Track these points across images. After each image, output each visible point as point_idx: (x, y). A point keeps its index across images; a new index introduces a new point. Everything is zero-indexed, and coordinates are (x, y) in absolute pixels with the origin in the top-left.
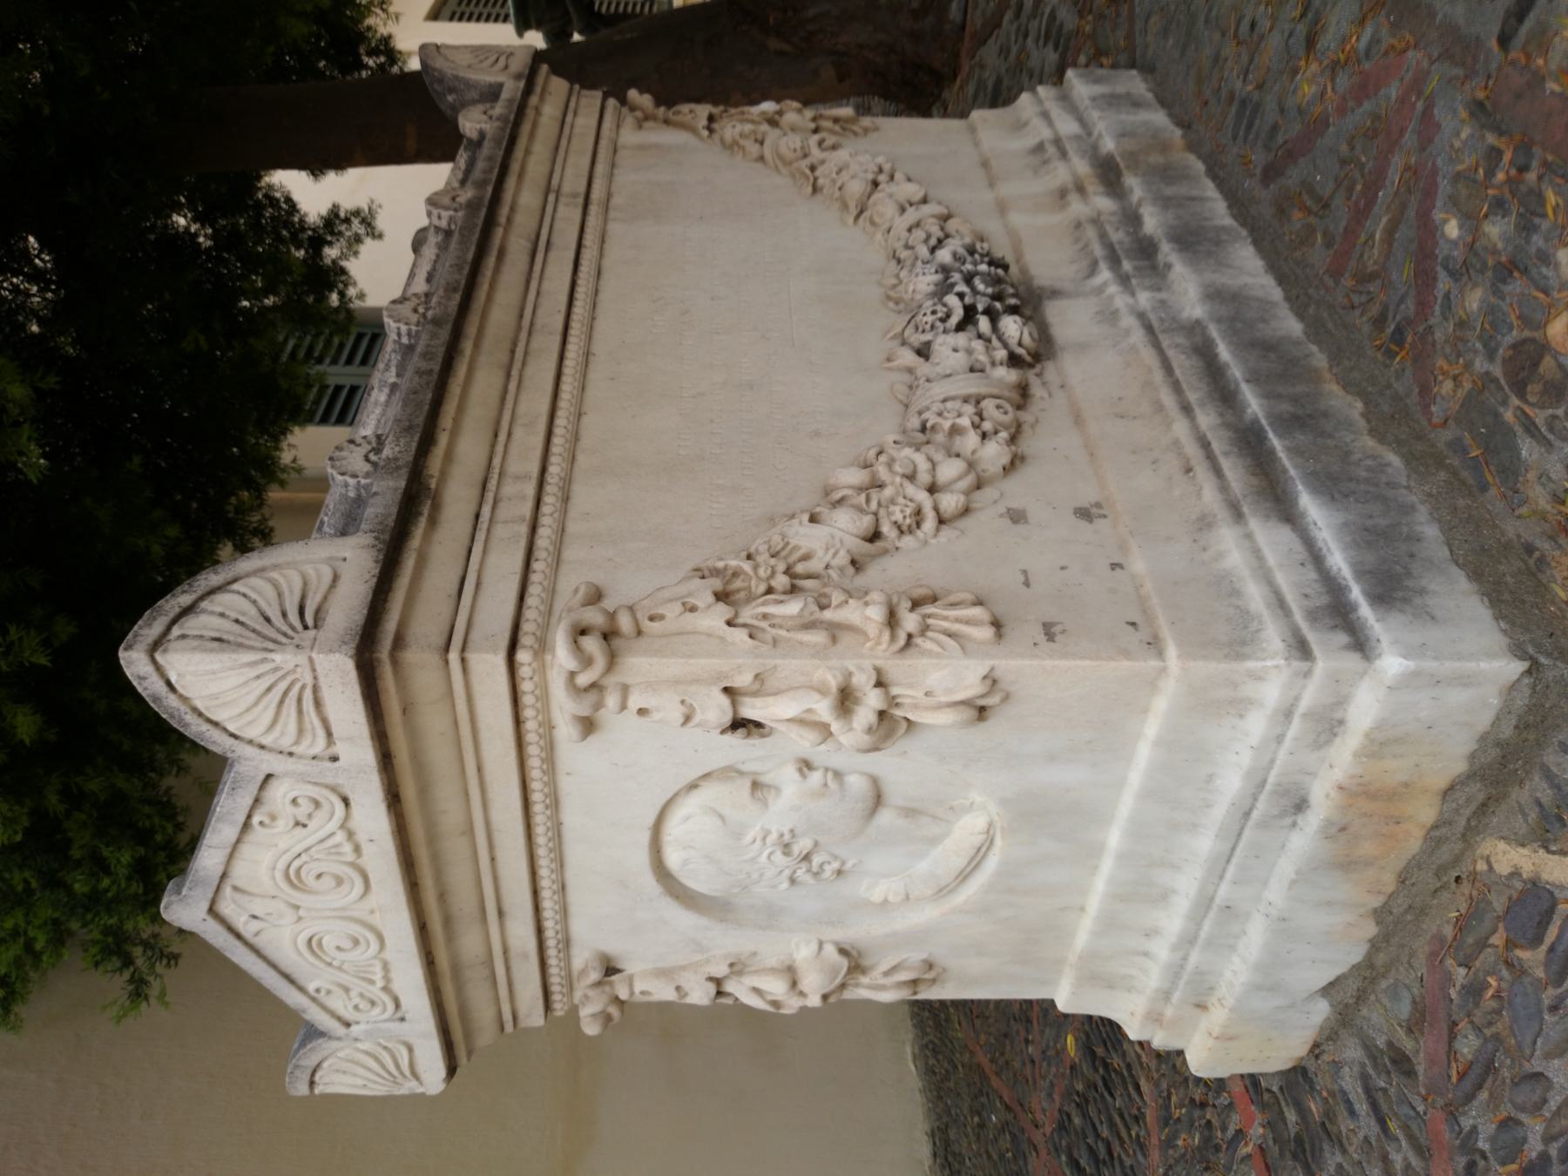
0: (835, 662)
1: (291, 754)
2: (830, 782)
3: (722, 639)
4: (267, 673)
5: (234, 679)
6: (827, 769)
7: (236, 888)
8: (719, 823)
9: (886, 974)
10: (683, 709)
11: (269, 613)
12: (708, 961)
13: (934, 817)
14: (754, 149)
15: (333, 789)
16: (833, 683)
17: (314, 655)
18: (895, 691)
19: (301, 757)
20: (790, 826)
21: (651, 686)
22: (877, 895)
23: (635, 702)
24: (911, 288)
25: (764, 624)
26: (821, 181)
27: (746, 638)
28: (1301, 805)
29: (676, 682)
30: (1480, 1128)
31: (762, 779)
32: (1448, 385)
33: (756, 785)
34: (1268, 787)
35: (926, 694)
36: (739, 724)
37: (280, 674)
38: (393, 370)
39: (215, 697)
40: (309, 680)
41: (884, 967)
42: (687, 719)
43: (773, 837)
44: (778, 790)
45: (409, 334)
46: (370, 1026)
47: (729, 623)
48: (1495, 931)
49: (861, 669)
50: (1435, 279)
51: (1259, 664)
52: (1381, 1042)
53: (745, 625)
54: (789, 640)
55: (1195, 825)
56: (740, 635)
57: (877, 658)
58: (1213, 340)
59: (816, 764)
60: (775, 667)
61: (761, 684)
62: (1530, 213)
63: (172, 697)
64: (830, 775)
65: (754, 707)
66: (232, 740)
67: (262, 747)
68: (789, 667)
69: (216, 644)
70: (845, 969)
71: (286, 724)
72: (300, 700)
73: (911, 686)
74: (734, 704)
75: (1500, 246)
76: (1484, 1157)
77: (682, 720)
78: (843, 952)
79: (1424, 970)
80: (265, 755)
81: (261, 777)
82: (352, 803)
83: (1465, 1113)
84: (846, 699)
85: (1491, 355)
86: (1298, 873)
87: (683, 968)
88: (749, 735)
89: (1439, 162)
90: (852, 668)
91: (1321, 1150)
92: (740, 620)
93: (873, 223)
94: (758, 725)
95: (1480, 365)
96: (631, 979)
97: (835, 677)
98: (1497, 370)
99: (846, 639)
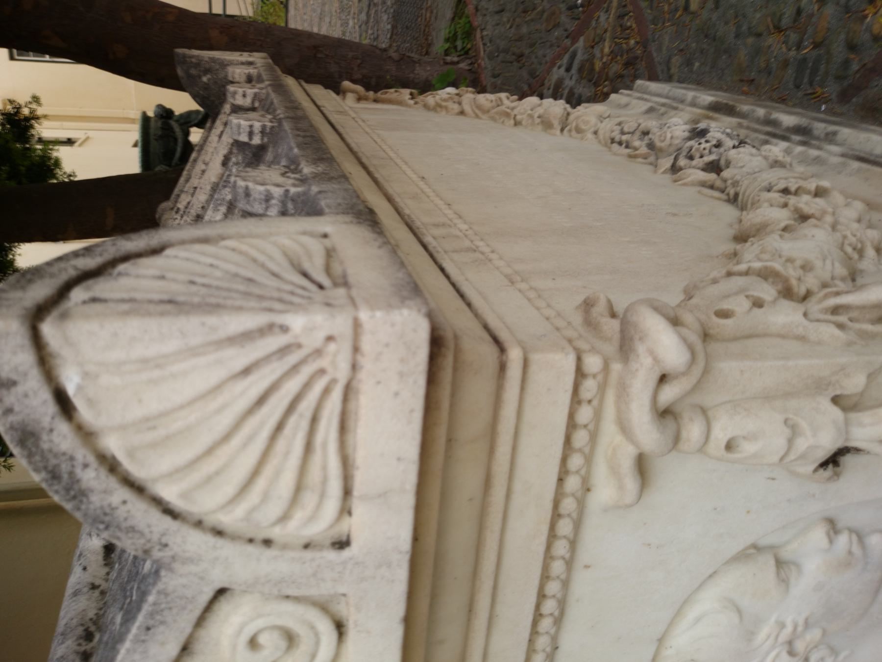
1: (267, 543)
4: (266, 359)
5: (204, 374)
11: (249, 274)
14: (456, 107)
15: (323, 607)
17: (364, 315)
19: (285, 547)
23: (720, 434)
24: (669, 135)
26: (519, 117)
33: (780, 563)
37: (292, 359)
39: (149, 422)
40: (342, 373)
44: (798, 566)
45: (263, 132)
63: (63, 427)
66: (167, 520)
67: (219, 533)
69: (168, 307)
71: (278, 473)
72: (314, 420)
80: (226, 549)
81: (208, 593)
93: (579, 130)
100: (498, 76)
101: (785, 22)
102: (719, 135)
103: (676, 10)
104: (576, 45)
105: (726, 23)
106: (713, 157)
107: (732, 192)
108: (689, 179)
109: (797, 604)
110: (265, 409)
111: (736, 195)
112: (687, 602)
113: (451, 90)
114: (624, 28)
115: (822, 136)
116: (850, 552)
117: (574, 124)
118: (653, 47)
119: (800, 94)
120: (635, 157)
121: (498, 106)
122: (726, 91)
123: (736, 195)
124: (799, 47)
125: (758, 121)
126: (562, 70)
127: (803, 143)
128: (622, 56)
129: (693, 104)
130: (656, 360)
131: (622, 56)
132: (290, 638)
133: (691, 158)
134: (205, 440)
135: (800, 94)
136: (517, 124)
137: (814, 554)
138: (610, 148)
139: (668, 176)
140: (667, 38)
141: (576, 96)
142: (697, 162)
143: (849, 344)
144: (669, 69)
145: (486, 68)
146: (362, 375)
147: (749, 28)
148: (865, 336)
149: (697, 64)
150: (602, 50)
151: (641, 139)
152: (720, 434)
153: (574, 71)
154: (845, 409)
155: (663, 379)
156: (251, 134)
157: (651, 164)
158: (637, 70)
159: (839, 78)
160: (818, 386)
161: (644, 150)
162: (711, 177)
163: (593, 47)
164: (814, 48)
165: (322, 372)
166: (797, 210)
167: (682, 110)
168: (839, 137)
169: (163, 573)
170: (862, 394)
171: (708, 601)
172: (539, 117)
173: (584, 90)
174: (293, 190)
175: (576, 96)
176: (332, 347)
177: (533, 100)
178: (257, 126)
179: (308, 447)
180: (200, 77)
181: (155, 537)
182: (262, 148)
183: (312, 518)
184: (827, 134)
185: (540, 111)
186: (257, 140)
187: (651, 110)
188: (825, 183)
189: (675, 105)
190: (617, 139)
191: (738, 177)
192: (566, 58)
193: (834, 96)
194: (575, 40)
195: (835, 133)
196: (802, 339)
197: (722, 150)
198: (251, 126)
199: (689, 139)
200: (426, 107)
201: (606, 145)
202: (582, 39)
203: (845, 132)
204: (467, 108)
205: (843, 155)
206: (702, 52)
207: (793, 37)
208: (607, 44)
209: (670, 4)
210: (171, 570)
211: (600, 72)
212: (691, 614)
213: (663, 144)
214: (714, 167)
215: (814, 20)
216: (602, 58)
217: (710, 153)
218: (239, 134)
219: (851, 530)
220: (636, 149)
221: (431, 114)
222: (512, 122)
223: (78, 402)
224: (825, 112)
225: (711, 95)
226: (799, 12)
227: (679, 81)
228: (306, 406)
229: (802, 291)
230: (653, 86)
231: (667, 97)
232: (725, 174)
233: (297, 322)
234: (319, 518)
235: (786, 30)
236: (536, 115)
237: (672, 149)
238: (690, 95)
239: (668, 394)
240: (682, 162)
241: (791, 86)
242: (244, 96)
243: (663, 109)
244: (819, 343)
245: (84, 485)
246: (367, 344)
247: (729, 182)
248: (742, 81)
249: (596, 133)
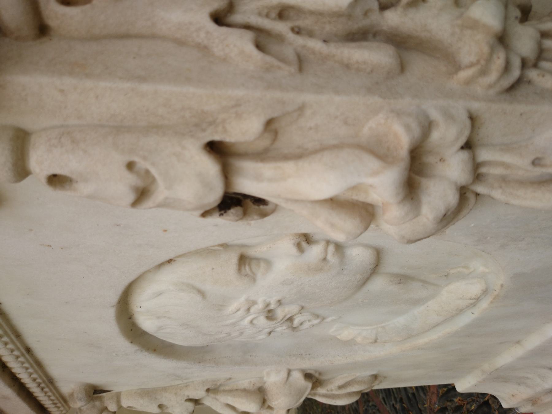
0: (406, 103)
2: (330, 257)
3: (204, 49)
6: (328, 242)
8: (198, 298)
9: (340, 387)
10: (131, 179)
13: (425, 282)
16: (402, 138)
18: (484, 155)
20: (279, 298)
21: (68, 136)
23: (41, 162)
25: (281, 27)
27: (250, 48)
29: (117, 129)
31: (251, 252)
35: (535, 162)
36: (232, 202)
41: (340, 382)
42: (142, 195)
43: (260, 306)
44: (268, 263)
47: (219, 19)
49: (449, 117)
53: (247, 27)
54: (324, 58)
56: (236, 44)
57: (476, 98)
59: (316, 237)
60: (301, 109)
61: (274, 143)
64: (331, 248)
65: (259, 178)
68: (326, 109)
70: (309, 389)
73: (507, 148)
74: (227, 173)
77: (131, 197)
78: (308, 376)
84: (415, 170)
87: (165, 389)
88: (245, 214)
90: (435, 115)
92: (237, 18)
94: (259, 201)
96: (118, 396)
97: (407, 128)
99: (419, 65)
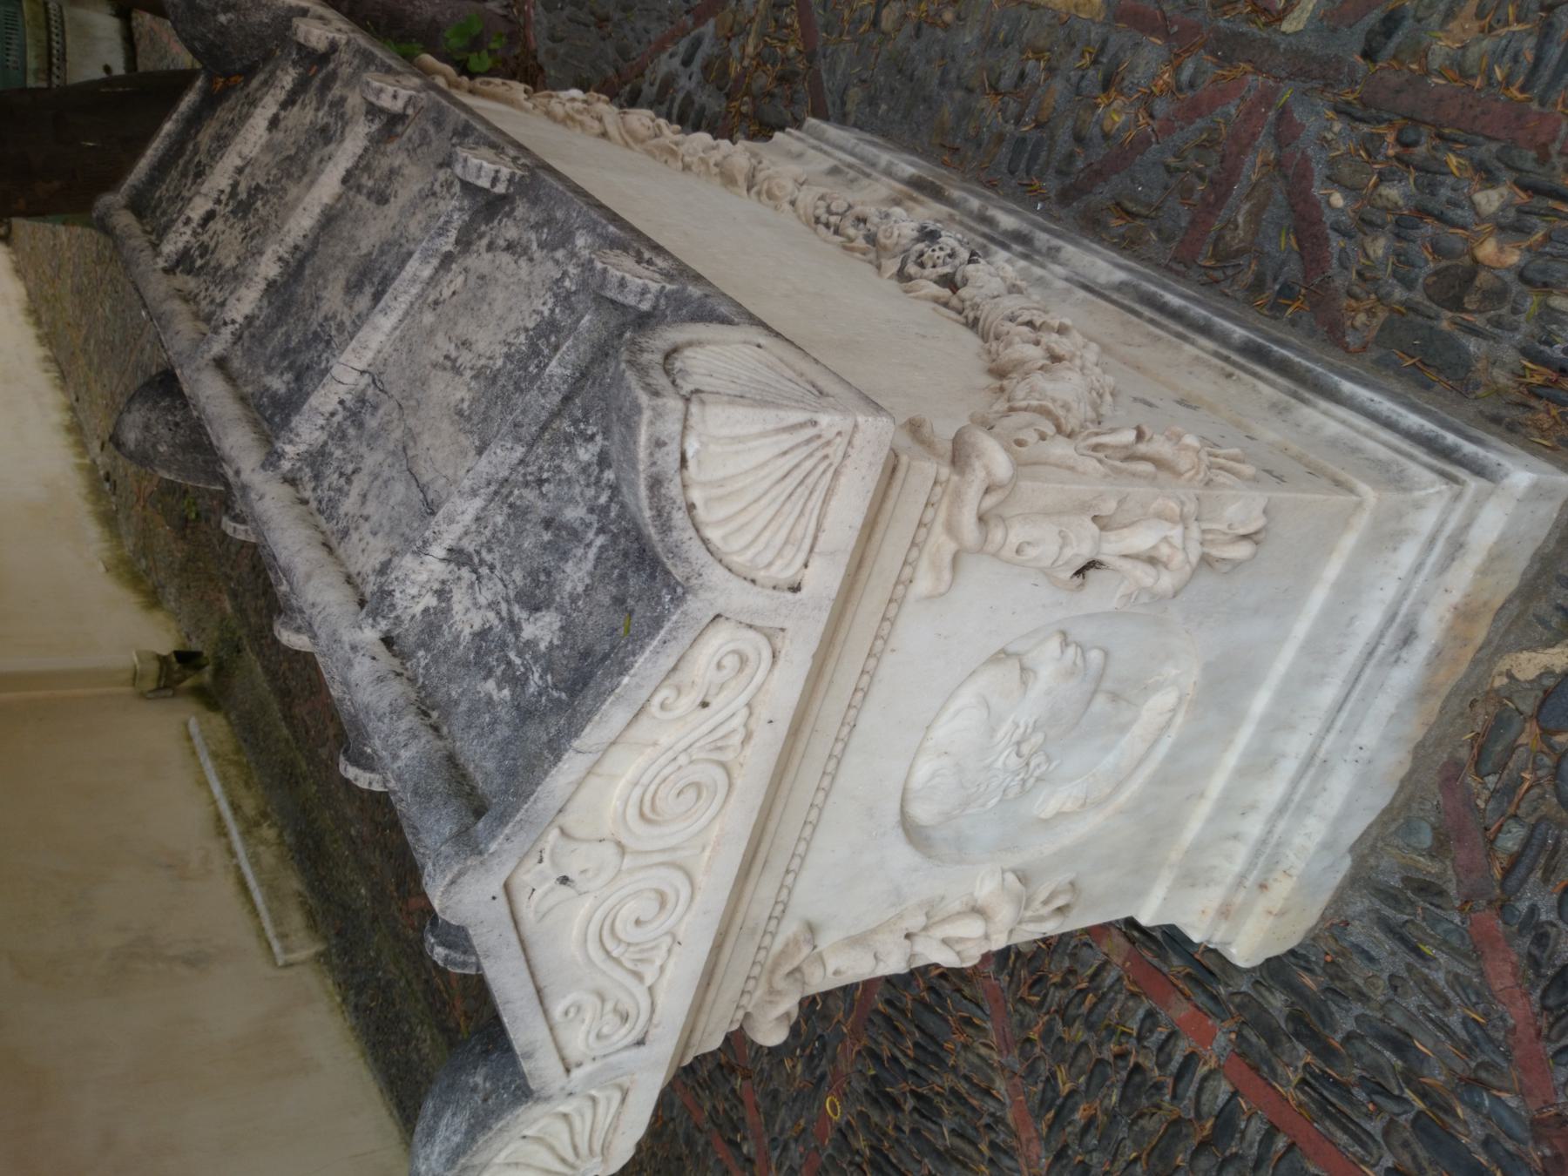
7: (563, 832)
9: (1045, 903)
12: (900, 916)
22: (1049, 810)
24: (896, 233)
28: (1408, 637)
30: (1540, 904)
32: (1361, 318)
33: (1023, 669)
34: (1399, 620)
38: (453, 234)
39: (720, 483)
40: (837, 460)
44: (1035, 673)
45: (510, 181)
46: (598, 1064)
48: (1522, 731)
50: (1327, 239)
51: (1423, 493)
52: (1395, 882)
55: (1323, 676)
58: (1154, 294)
62: (1430, 173)
75: (1401, 203)
76: (1554, 925)
79: (1440, 797)
82: (781, 662)
83: (1519, 899)
85: (1409, 284)
86: (1398, 707)
87: (874, 931)
89: (1310, 152)
91: (1331, 1014)
93: (770, 195)
95: (1399, 293)
98: (1418, 296)
100: (562, 40)
101: (1005, 83)
102: (953, 243)
103: (861, 22)
104: (702, 29)
105: (929, 62)
106: (947, 269)
107: (971, 316)
108: (922, 292)
109: (1028, 710)
110: (788, 480)
111: (976, 320)
112: (951, 696)
113: (575, 93)
114: (780, 25)
115: (1044, 250)
116: (1075, 663)
117: (765, 187)
118: (822, 65)
119: (1014, 182)
120: (852, 249)
121: (656, 136)
122: (920, 155)
123: (976, 320)
124: (1018, 121)
125: (970, 214)
126: (676, 62)
127: (1026, 257)
128: (773, 65)
129: (888, 172)
130: (989, 474)
131: (773, 65)
132: (743, 660)
133: (922, 265)
134: (749, 497)
135: (1014, 182)
136: (687, 168)
137: (1049, 661)
138: (815, 230)
139: (894, 283)
140: (844, 57)
141: (696, 106)
142: (928, 271)
143: (1106, 476)
144: (843, 103)
145: (538, 22)
146: (848, 462)
147: (959, 78)
148: (1114, 469)
149: (884, 107)
150: (743, 48)
151: (855, 226)
152: (1015, 538)
153: (696, 66)
154: (1103, 528)
155: (987, 491)
156: (495, 181)
157: (870, 262)
158: (796, 92)
159: (1060, 172)
160: (1082, 507)
161: (861, 243)
162: (945, 293)
163: (729, 39)
164: (1037, 127)
165: (826, 457)
166: (1049, 350)
167: (877, 180)
168: (1063, 255)
169: (689, 597)
170: (1110, 517)
171: (967, 696)
172: (716, 165)
173: (710, 101)
174: (669, 287)
175: (696, 106)
176: (839, 439)
177: (703, 138)
178: (505, 172)
179: (802, 513)
180: (215, 14)
181: (697, 568)
182: (503, 198)
183: (788, 565)
184: (1050, 249)
185: (716, 156)
186: (500, 189)
187: (834, 171)
188: (1068, 322)
189: (868, 170)
190: (824, 217)
191: (978, 300)
192: (683, 45)
193: (1052, 195)
194: (700, 20)
195: (1058, 249)
196: (1072, 469)
197: (957, 262)
198: (497, 172)
199: (918, 240)
200: (549, 114)
201: (808, 224)
202: (712, 22)
203: (1069, 250)
204: (612, 131)
205: (1067, 279)
206: (892, 92)
207: (1013, 107)
208: (751, 41)
209: (852, 11)
210: (695, 595)
211: (736, 81)
212: (953, 707)
213: (888, 242)
214: (949, 282)
215: (1039, 91)
216: (742, 58)
217: (944, 264)
218: (479, 177)
219: (1078, 645)
220: (851, 240)
221: (559, 128)
222: (680, 164)
223: (691, 464)
224: (1040, 213)
225: (912, 164)
226: (1022, 76)
227: (855, 125)
228: (810, 481)
229: (1069, 430)
230: (832, 131)
231: (852, 154)
232: (963, 292)
233: (824, 419)
234: (784, 572)
235: (1004, 94)
236: (712, 162)
237: (897, 250)
238: (885, 158)
239: (990, 501)
240: (912, 269)
241: (1004, 168)
242: (395, 97)
243: (852, 174)
244: (1084, 473)
245: (673, 523)
246: (857, 441)
247: (968, 303)
248: (943, 146)
249: (793, 203)
